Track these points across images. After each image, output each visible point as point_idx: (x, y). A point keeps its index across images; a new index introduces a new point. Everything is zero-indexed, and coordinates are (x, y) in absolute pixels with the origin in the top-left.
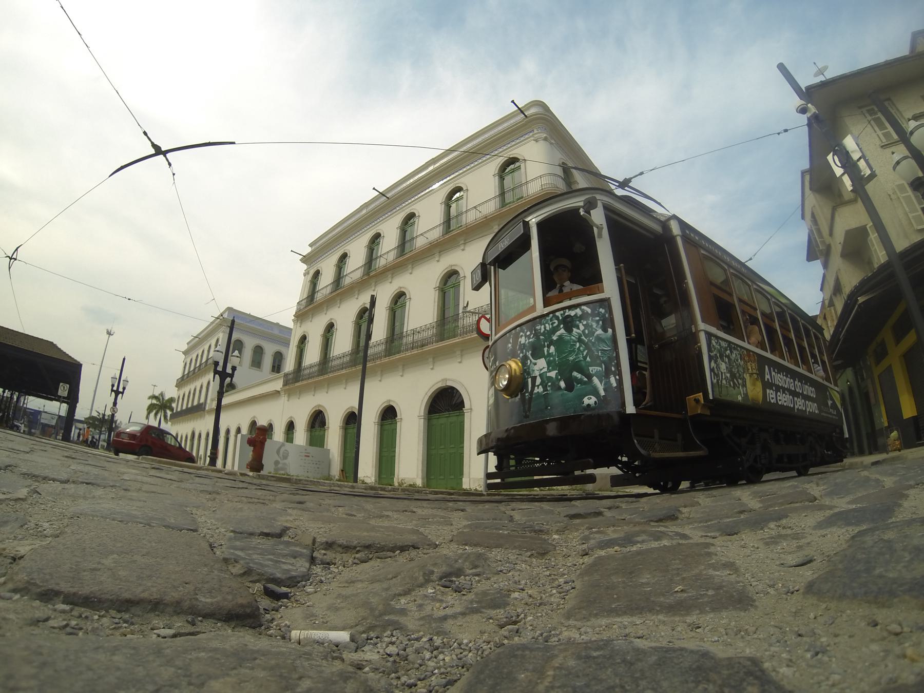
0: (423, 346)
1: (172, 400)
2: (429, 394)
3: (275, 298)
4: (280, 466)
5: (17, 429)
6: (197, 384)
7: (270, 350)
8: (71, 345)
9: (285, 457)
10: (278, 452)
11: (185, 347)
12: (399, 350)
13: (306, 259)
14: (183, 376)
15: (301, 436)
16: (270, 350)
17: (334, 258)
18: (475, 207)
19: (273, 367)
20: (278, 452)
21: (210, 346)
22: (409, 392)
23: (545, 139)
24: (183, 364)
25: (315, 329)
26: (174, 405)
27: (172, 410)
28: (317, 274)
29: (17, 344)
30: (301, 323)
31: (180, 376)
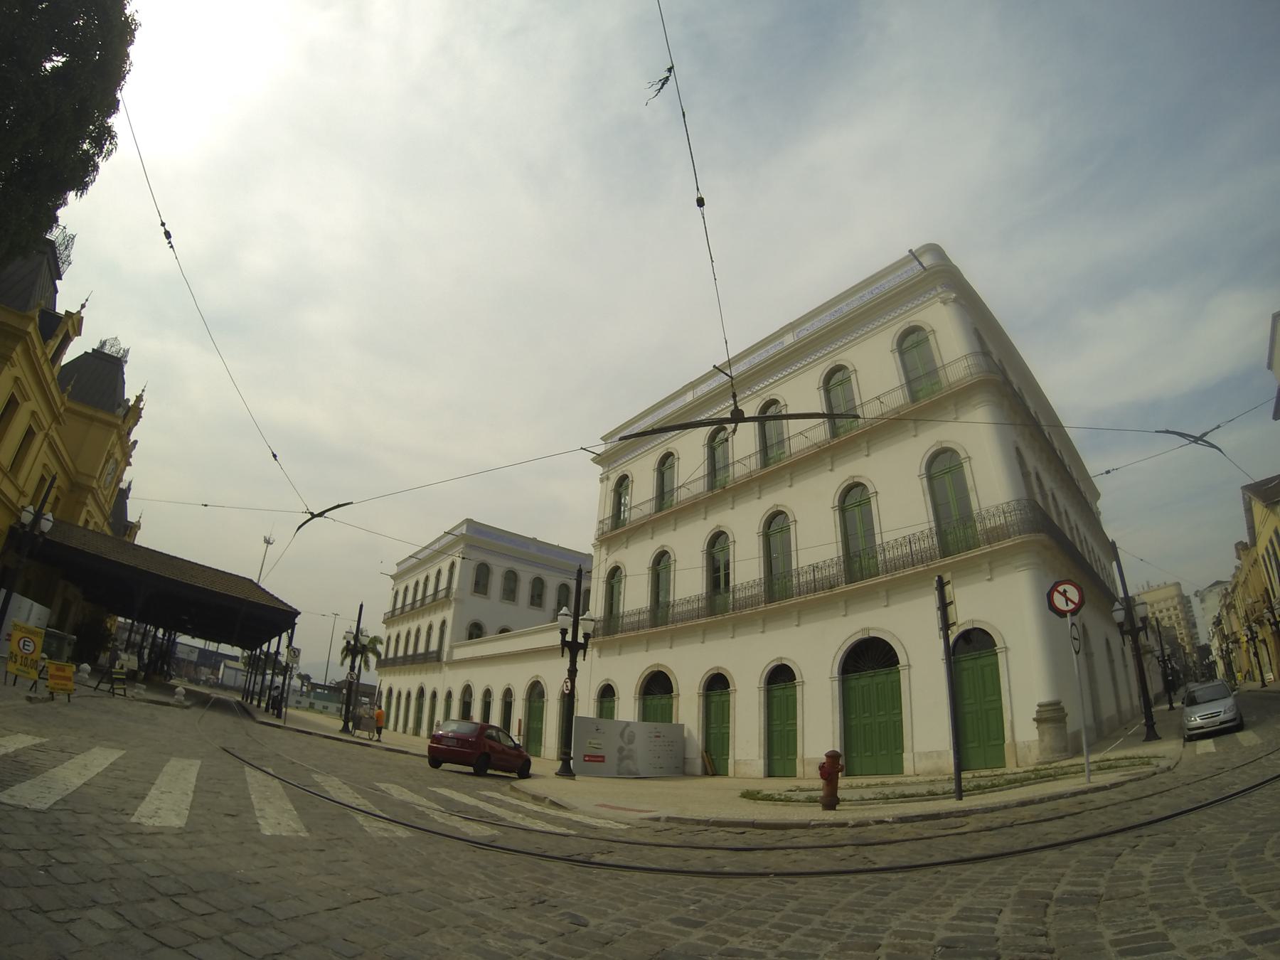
0: (832, 587)
1: (376, 640)
2: (845, 648)
3: (566, 512)
4: (625, 753)
5: (171, 690)
6: (423, 623)
7: (526, 577)
8: (280, 586)
9: (631, 741)
10: (622, 735)
11: (394, 570)
12: (781, 591)
13: (600, 459)
14: (394, 609)
15: (627, 708)
16: (526, 577)
17: (652, 459)
18: (878, 398)
19: (477, 584)
20: (622, 735)
21: (439, 572)
22: (816, 648)
23: (955, 300)
24: (392, 594)
25: (636, 560)
26: (381, 648)
27: (378, 655)
28: (623, 482)
29: (167, 574)
30: (608, 549)
31: (389, 608)
